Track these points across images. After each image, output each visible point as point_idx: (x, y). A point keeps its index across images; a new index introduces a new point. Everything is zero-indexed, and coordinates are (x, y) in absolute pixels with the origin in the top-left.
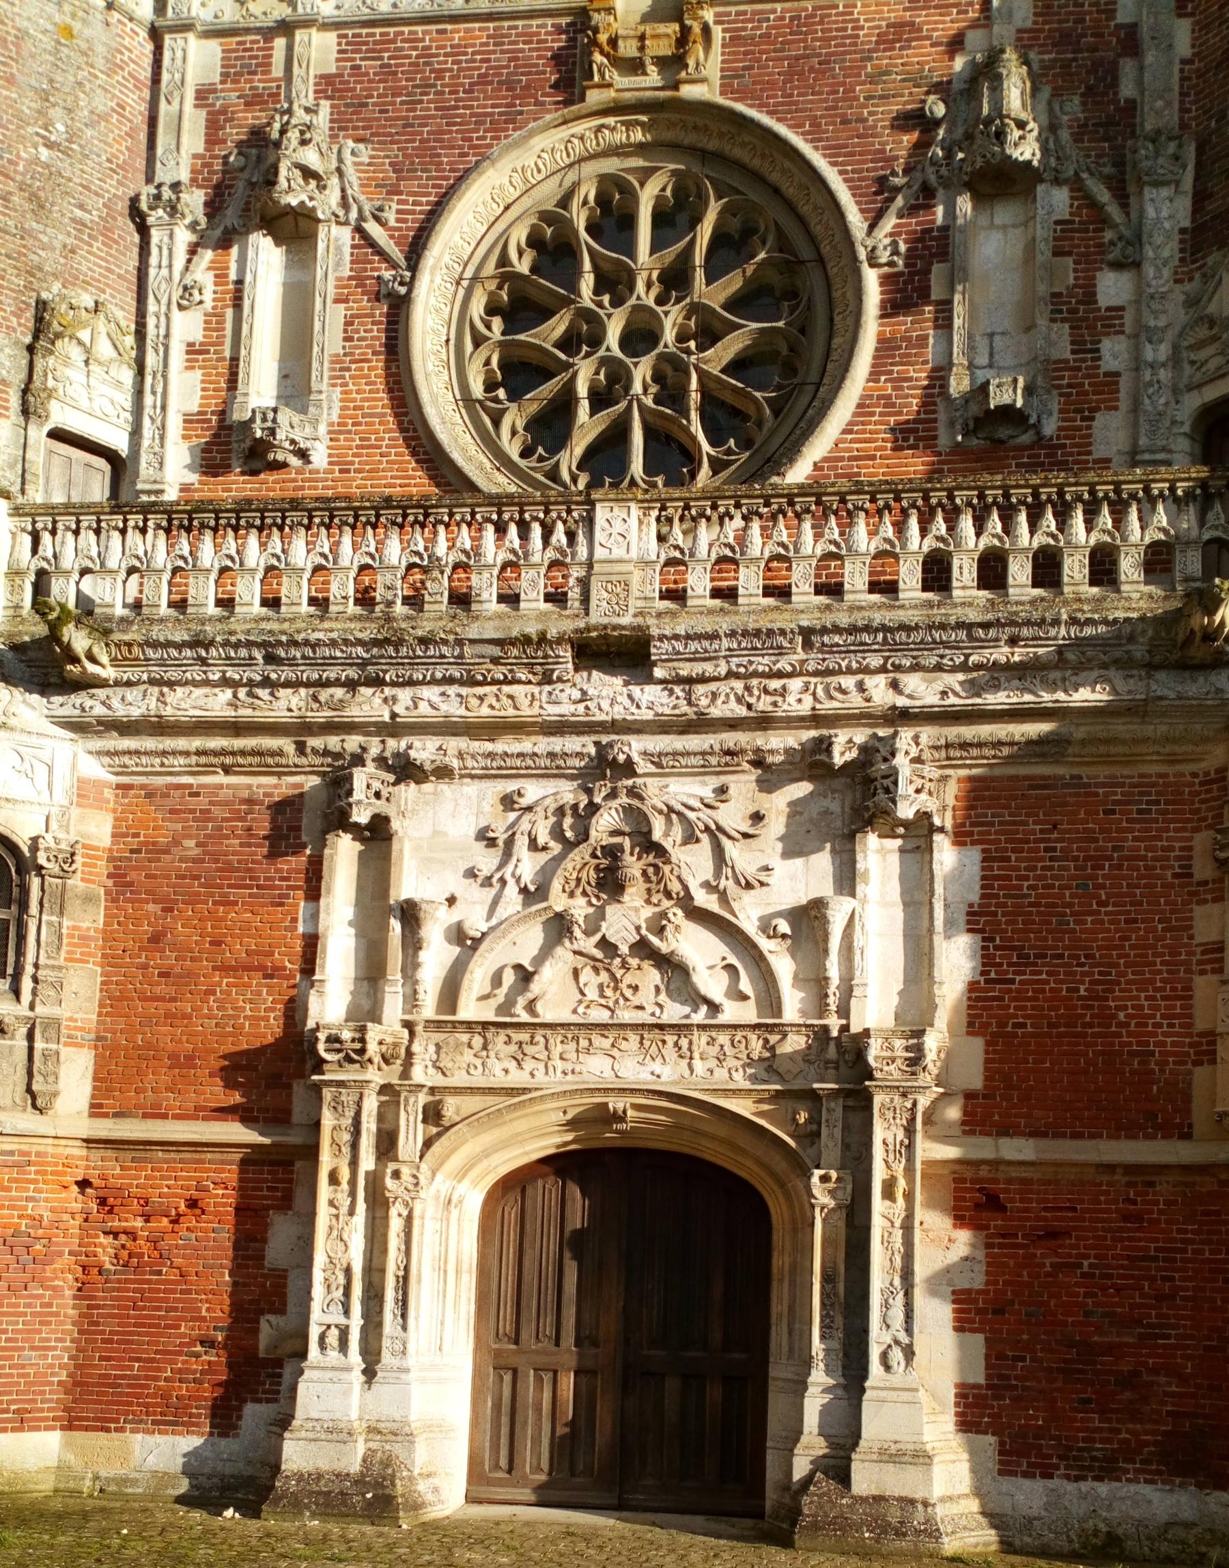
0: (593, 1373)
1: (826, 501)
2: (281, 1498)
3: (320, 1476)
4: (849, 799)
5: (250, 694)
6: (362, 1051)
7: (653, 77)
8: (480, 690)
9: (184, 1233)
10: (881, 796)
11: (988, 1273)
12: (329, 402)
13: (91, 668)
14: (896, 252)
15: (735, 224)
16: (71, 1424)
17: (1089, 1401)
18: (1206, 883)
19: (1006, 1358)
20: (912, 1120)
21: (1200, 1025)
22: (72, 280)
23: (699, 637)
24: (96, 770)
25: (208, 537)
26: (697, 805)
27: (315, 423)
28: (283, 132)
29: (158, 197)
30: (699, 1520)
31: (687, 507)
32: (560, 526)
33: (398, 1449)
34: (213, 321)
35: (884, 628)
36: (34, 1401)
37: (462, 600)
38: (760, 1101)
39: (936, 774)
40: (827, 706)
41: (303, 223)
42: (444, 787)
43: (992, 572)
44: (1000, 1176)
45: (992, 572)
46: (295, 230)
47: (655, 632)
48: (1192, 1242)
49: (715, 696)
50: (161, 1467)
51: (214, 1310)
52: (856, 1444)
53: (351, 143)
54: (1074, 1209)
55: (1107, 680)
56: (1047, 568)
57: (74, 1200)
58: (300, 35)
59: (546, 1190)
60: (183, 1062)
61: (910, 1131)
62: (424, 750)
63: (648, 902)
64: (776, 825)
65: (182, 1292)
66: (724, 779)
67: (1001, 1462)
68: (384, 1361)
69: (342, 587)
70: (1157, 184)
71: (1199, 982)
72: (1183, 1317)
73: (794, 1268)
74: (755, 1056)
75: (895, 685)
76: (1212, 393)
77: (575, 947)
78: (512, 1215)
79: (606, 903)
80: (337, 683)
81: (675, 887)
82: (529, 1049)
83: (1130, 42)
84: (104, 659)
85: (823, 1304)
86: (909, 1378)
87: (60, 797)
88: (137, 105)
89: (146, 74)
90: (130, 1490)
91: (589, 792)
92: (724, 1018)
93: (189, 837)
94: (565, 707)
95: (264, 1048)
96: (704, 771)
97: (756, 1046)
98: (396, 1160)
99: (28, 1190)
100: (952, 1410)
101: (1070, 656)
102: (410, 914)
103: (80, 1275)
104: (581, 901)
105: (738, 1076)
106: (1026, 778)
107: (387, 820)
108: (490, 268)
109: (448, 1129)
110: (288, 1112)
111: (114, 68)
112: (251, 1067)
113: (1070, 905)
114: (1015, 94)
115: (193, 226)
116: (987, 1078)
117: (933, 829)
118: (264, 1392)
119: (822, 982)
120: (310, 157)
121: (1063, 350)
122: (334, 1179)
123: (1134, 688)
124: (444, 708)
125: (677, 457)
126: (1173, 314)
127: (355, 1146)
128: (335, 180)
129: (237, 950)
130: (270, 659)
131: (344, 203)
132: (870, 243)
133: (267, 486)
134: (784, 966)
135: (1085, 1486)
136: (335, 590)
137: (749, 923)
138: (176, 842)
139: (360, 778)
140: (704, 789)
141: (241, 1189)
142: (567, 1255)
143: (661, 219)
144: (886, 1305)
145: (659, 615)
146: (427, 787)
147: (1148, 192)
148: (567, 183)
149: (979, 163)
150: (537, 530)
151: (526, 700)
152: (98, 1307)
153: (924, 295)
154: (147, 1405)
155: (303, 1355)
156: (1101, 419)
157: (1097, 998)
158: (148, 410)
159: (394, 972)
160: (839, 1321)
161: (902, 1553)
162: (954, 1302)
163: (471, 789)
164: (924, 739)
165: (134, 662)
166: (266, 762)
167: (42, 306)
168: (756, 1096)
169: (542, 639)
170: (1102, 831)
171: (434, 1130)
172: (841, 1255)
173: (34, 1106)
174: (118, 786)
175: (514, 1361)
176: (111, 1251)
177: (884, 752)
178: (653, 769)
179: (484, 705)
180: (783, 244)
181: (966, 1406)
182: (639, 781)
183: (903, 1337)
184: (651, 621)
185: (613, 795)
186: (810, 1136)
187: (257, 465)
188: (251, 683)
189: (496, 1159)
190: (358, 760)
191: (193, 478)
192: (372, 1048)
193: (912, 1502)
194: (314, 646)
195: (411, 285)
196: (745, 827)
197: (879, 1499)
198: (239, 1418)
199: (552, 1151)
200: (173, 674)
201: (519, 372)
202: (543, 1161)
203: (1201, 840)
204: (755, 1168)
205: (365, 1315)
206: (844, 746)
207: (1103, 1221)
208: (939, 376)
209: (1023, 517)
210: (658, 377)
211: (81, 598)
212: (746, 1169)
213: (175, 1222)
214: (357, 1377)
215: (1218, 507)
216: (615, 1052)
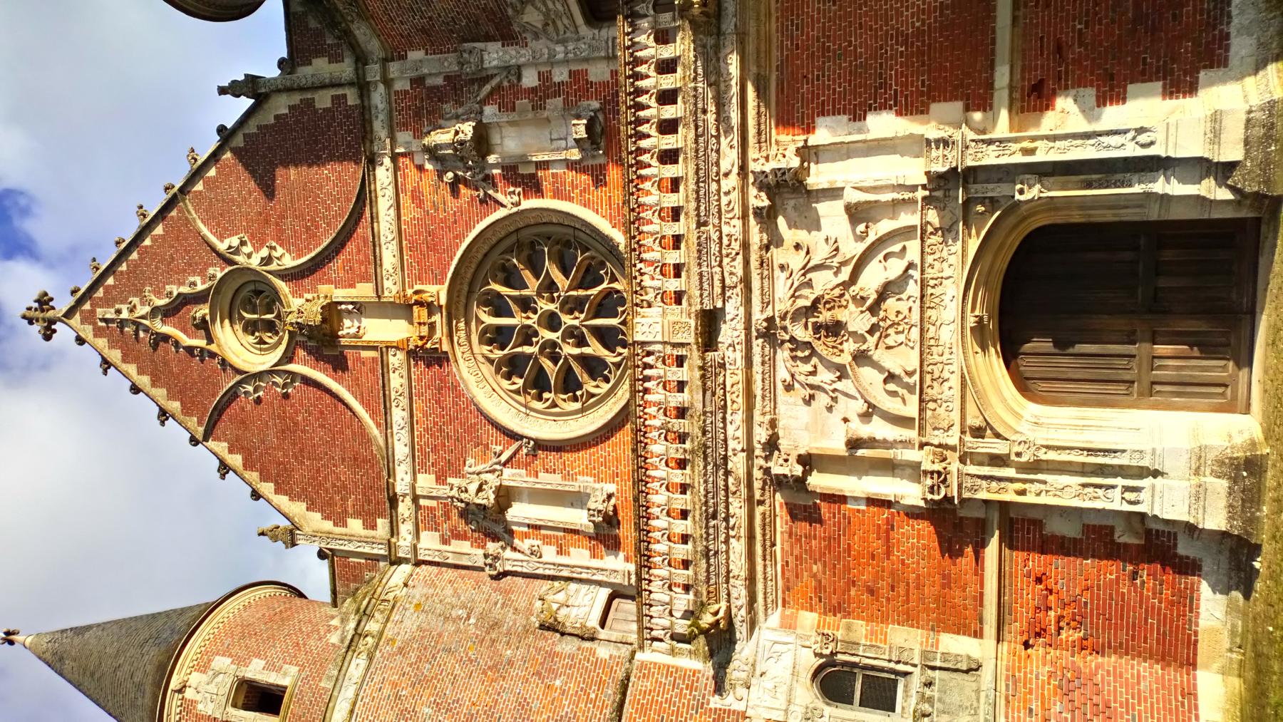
0: (1154, 333)
2: (1246, 531)
3: (1231, 506)
4: (788, 194)
5: (733, 529)
6: (939, 473)
7: (437, 318)
8: (729, 403)
10: (787, 177)
11: (1085, 86)
12: (583, 482)
13: (721, 614)
14: (514, 193)
15: (501, 275)
16: (1192, 664)
17: (1174, 16)
19: (1144, 70)
20: (983, 141)
23: (701, 283)
24: (775, 618)
28: (462, 501)
29: (491, 565)
30: (1262, 261)
31: (636, 292)
32: (646, 360)
33: (1211, 456)
34: (547, 540)
35: (697, 183)
36: (1176, 686)
37: (681, 412)
38: (970, 235)
39: (774, 147)
40: (738, 211)
46: (506, 496)
47: (699, 307)
49: (731, 273)
51: (1111, 571)
53: (466, 468)
54: (1042, 38)
56: (667, 97)
57: (1037, 652)
58: (419, 492)
59: (1027, 365)
60: (947, 581)
61: (990, 142)
62: (761, 435)
63: (846, 307)
64: (801, 236)
66: (776, 267)
67: (1218, 67)
68: (1147, 464)
69: (678, 476)
70: (482, 61)
73: (1081, 208)
74: (941, 240)
77: (873, 348)
78: (1044, 386)
80: (726, 480)
81: (837, 292)
82: (936, 375)
84: (716, 607)
85: (1107, 187)
86: (1159, 129)
87: (791, 639)
88: (450, 574)
89: (435, 569)
91: (783, 342)
92: (917, 261)
93: (811, 568)
94: (737, 356)
95: (937, 533)
96: (771, 278)
97: (936, 239)
99: (1031, 679)
101: (713, 79)
102: (854, 444)
103: (1088, 652)
105: (953, 249)
106: (777, 96)
107: (800, 456)
110: (978, 519)
112: (950, 541)
113: (851, 62)
115: (503, 548)
116: (956, 99)
119: (895, 203)
120: (473, 488)
121: (559, 101)
122: (1022, 493)
123: (730, 41)
126: (541, 46)
127: (1000, 479)
129: (878, 545)
130: (714, 517)
131: (493, 471)
132: (510, 206)
133: (626, 517)
134: (884, 226)
135: (1234, 11)
137: (861, 247)
139: (776, 470)
140: (780, 277)
142: (1071, 351)
143: (497, 314)
146: (781, 434)
147: (486, 65)
148: (482, 360)
149: (474, 153)
152: (1109, 643)
153: (533, 176)
154: (1178, 615)
155: (1142, 515)
156: (592, 78)
157: (907, 39)
158: (589, 577)
160: (1119, 176)
162: (1105, 105)
163: (781, 408)
164: (756, 156)
166: (769, 522)
167: (542, 627)
169: (702, 368)
170: (808, 49)
171: (989, 431)
173: (977, 670)
174: (784, 606)
175: (1146, 384)
176: (1071, 632)
177: (762, 178)
178: (770, 307)
179: (737, 401)
180: (509, 250)
181: (1178, 92)
184: (693, 310)
185: (785, 329)
186: (993, 203)
187: (615, 522)
188: (727, 528)
190: (767, 471)
191: (621, 555)
192: (938, 467)
193: (1248, 121)
195: (529, 439)
196: (803, 253)
198: (1187, 557)
200: (723, 570)
201: (569, 384)
204: (1014, 235)
205: (1115, 476)
206: (759, 200)
208: (571, 165)
209: (641, 114)
210: (571, 312)
211: (683, 617)
212: (1014, 241)
213: (1051, 592)
215: (637, 8)
216: (938, 324)
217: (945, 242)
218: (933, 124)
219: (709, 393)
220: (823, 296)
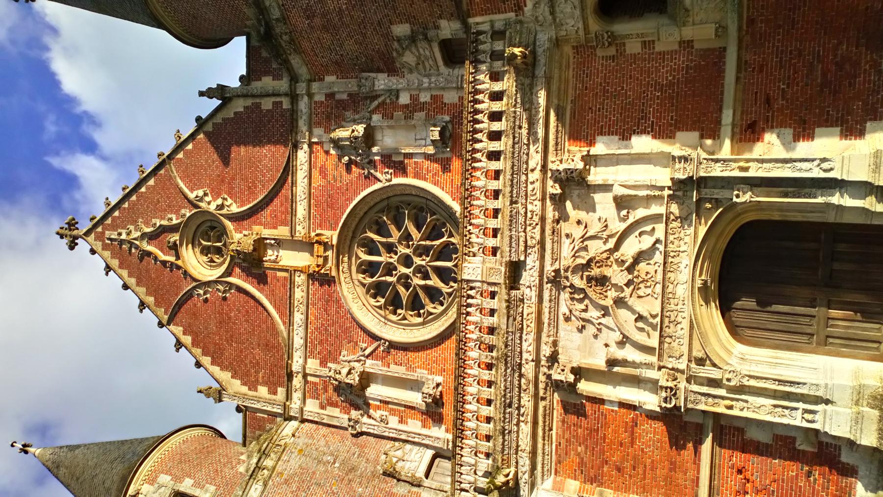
4: (574, 186)
5: (523, 416)
6: (671, 389)
7: (329, 253)
10: (574, 175)
11: (786, 127)
12: (420, 373)
13: (511, 476)
15: (375, 227)
17: (850, 83)
18: (617, 50)
20: (712, 160)
21: (676, 47)
23: (511, 243)
24: (549, 482)
26: (572, 246)
27: (428, 379)
28: (336, 380)
29: (352, 427)
31: (466, 246)
32: (469, 292)
33: (868, 392)
34: (393, 412)
35: (512, 175)
37: (491, 331)
38: (700, 224)
40: (539, 195)
42: (560, 344)
46: (366, 379)
47: (508, 259)
48: (774, 44)
49: (532, 237)
51: (792, 469)
52: (870, 183)
53: (341, 357)
54: (756, 93)
58: (307, 371)
59: (737, 317)
61: (717, 161)
62: (546, 350)
63: (611, 266)
64: (582, 215)
66: (563, 235)
69: (486, 375)
70: (374, 85)
71: (657, 49)
72: (810, 45)
74: (680, 225)
75: (532, 170)
76: (440, 62)
78: (749, 332)
79: (610, 283)
80: (520, 381)
81: (605, 255)
82: (672, 319)
83: (330, 96)
84: (507, 471)
85: (798, 197)
88: (324, 430)
89: (314, 426)
91: (565, 287)
92: (663, 238)
93: (577, 449)
94: (532, 294)
95: (667, 431)
96: (559, 242)
101: (527, 106)
102: (612, 362)
104: (609, 293)
105: (688, 232)
107: (572, 368)
108: (382, 312)
109: (708, 356)
110: (698, 424)
111: (312, 437)
113: (622, 101)
114: (342, 133)
115: (362, 415)
116: (694, 130)
117: (588, 155)
120: (344, 371)
121: (422, 115)
122: (730, 407)
123: (541, 81)
124: (531, 341)
126: (414, 78)
127: (715, 397)
128: (352, 364)
129: (625, 437)
130: (510, 406)
134: (640, 213)
136: (486, 378)
137: (623, 226)
139: (556, 377)
140: (566, 242)
141: (733, 449)
142: (769, 309)
143: (370, 253)
144: (800, 170)
145: (502, 257)
146: (560, 351)
147: (376, 88)
153: (402, 162)
155: (817, 431)
156: (446, 101)
158: (420, 441)
160: (807, 190)
163: (561, 333)
164: (553, 159)
165: (509, 459)
167: (385, 474)
168: (698, 225)
169: (508, 301)
171: (708, 362)
174: (556, 474)
175: (823, 337)
178: (558, 262)
180: (382, 211)
181: (851, 135)
182: (562, 268)
184: (504, 260)
185: (567, 278)
186: (717, 203)
187: (440, 403)
188: (518, 415)
189: (722, 336)
190: (549, 377)
191: (443, 427)
192: (670, 384)
194: (506, 388)
195: (386, 340)
196: (582, 227)
198: (848, 464)
199: (719, 312)
200: (514, 445)
201: (416, 305)
202: (723, 317)
203: (600, 53)
205: (798, 401)
206: (554, 189)
207: (762, 81)
208: (427, 157)
209: (477, 126)
210: (420, 255)
213: (748, 481)
214: (829, 407)
215: (479, 57)
216: (675, 283)
217: (682, 227)
218: (678, 145)
219: (511, 319)
220: (595, 258)
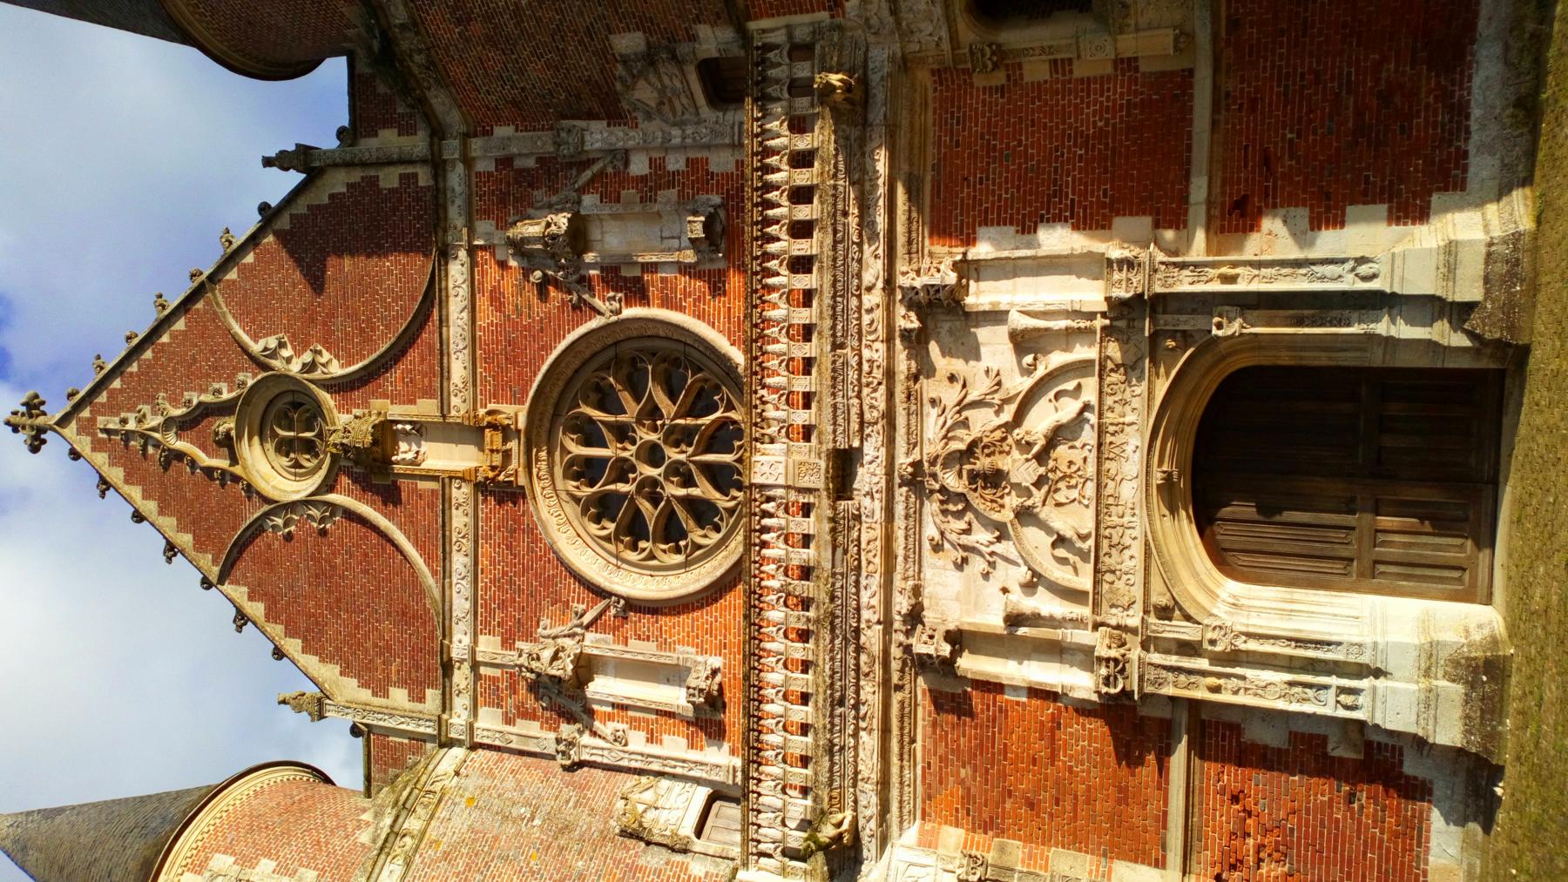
1: (755, 337)
2: (1486, 749)
3: (1467, 717)
4: (942, 316)
5: (864, 719)
6: (1116, 661)
7: (513, 445)
8: (864, 563)
9: (1259, 808)
10: (941, 295)
12: (684, 653)
13: (845, 826)
14: (613, 298)
15: (594, 397)
17: (1402, 127)
18: (1008, 77)
20: (1175, 264)
21: (1109, 70)
22: (608, 812)
23: (835, 417)
24: (912, 833)
25: (764, 737)
27: (697, 663)
28: (532, 671)
29: (564, 753)
30: (1506, 421)
31: (756, 424)
32: (764, 506)
33: (1444, 654)
34: (635, 724)
35: (834, 297)
37: (806, 572)
38: (1158, 375)
39: (927, 260)
40: (881, 333)
41: (582, 663)
42: (926, 592)
43: (801, 230)
44: (1219, 200)
45: (801, 230)
46: (587, 667)
47: (831, 446)
49: (872, 407)
50: (1458, 843)
51: (1322, 791)
52: (1439, 299)
54: (1246, 147)
55: (872, 152)
56: (801, 195)
58: (479, 658)
59: (1225, 533)
60: (1124, 796)
62: (902, 604)
63: (1008, 453)
64: (957, 365)
65: (1308, 813)
66: (925, 401)
67: (1455, 189)
69: (798, 651)
70: (583, 142)
73: (1292, 348)
74: (1123, 378)
75: (869, 289)
76: (701, 100)
78: (1245, 559)
80: (857, 659)
81: (998, 434)
82: (1115, 540)
83: (505, 162)
84: (840, 816)
85: (1321, 325)
88: (512, 762)
89: (494, 755)
90: (1478, 870)
91: (932, 492)
92: (1094, 400)
95: (1113, 734)
96: (920, 414)
97: (1115, 377)
98: (1201, 642)
100: (1410, 227)
104: (1007, 500)
105: (1138, 390)
107: (948, 632)
109: (1176, 603)
110: (1162, 721)
112: (1128, 745)
113: (1020, 165)
115: (581, 732)
116: (1144, 213)
118: (1393, 757)
119: (1069, 332)
120: (547, 655)
121: (672, 193)
122: (1216, 689)
123: (878, 133)
124: (874, 588)
125: (722, 433)
126: (654, 128)
127: (1190, 672)
129: (1040, 748)
130: (841, 703)
131: (572, 636)
133: (734, 697)
134: (1057, 359)
135: (1474, 127)
137: (1027, 383)
138: (962, 782)
139: (920, 648)
140: (932, 414)
142: (1277, 518)
143: (587, 443)
144: (1322, 278)
146: (926, 603)
150: (766, 521)
151: (870, 533)
153: (639, 280)
154: (1404, 850)
155: (1361, 724)
156: (713, 168)
158: (685, 772)
159: (1058, 634)
160: (1335, 313)
161: (1534, 261)
162: (1319, 229)
163: (928, 573)
164: (904, 269)
165: (842, 796)
167: (624, 833)
169: (832, 520)
171: (1177, 612)
172: (1282, 313)
174: (923, 818)
175: (1367, 563)
177: (912, 294)
178: (917, 449)
179: (874, 561)
180: (606, 367)
181: (1406, 217)
182: (925, 458)
183: (1351, 264)
184: (824, 448)
185: (934, 476)
186: (1185, 338)
187: (719, 704)
188: (857, 718)
190: (907, 649)
191: (726, 746)
192: (1114, 653)
193: (1489, 255)
195: (619, 597)
196: (958, 386)
197: (1487, 280)
198: (1415, 778)
200: (850, 771)
201: (671, 532)
205: (1329, 673)
206: (907, 320)
208: (684, 269)
209: (770, 212)
210: (676, 444)
212: (1211, 384)
213: (1250, 814)
214: (1381, 683)
216: (1118, 478)
217: (1128, 381)
219: (839, 551)
220: (981, 439)
